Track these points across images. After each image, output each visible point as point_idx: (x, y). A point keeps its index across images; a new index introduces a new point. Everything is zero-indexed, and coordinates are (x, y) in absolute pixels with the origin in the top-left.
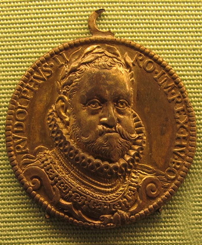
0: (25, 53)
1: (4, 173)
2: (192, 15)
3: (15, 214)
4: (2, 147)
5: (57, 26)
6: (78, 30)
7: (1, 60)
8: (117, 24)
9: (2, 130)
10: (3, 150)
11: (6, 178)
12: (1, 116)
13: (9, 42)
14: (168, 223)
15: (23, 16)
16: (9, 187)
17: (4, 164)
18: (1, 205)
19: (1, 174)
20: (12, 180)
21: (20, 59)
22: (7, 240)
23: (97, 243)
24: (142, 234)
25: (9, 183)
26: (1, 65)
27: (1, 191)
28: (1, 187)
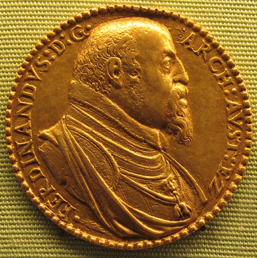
0: (236, 27)
1: (4, 186)
2: (8, 76)
3: (30, 231)
4: (2, 106)
5: (236, 9)
6: (6, 77)
7: (1, 3)
8: (239, 46)
9: (2, 125)
10: (3, 161)
11: (8, 186)
12: (1, 158)
13: (7, 72)
14: (247, 190)
15: (27, 36)
16: (17, 191)
17: (5, 167)
18: (1, 245)
19: (1, 176)
20: (31, 222)
21: (237, 42)
22: (10, 211)
23: (186, 240)
24: (230, 210)
25: (17, 206)
26: (1, 212)
27: (1, 158)
28: (1, 172)
